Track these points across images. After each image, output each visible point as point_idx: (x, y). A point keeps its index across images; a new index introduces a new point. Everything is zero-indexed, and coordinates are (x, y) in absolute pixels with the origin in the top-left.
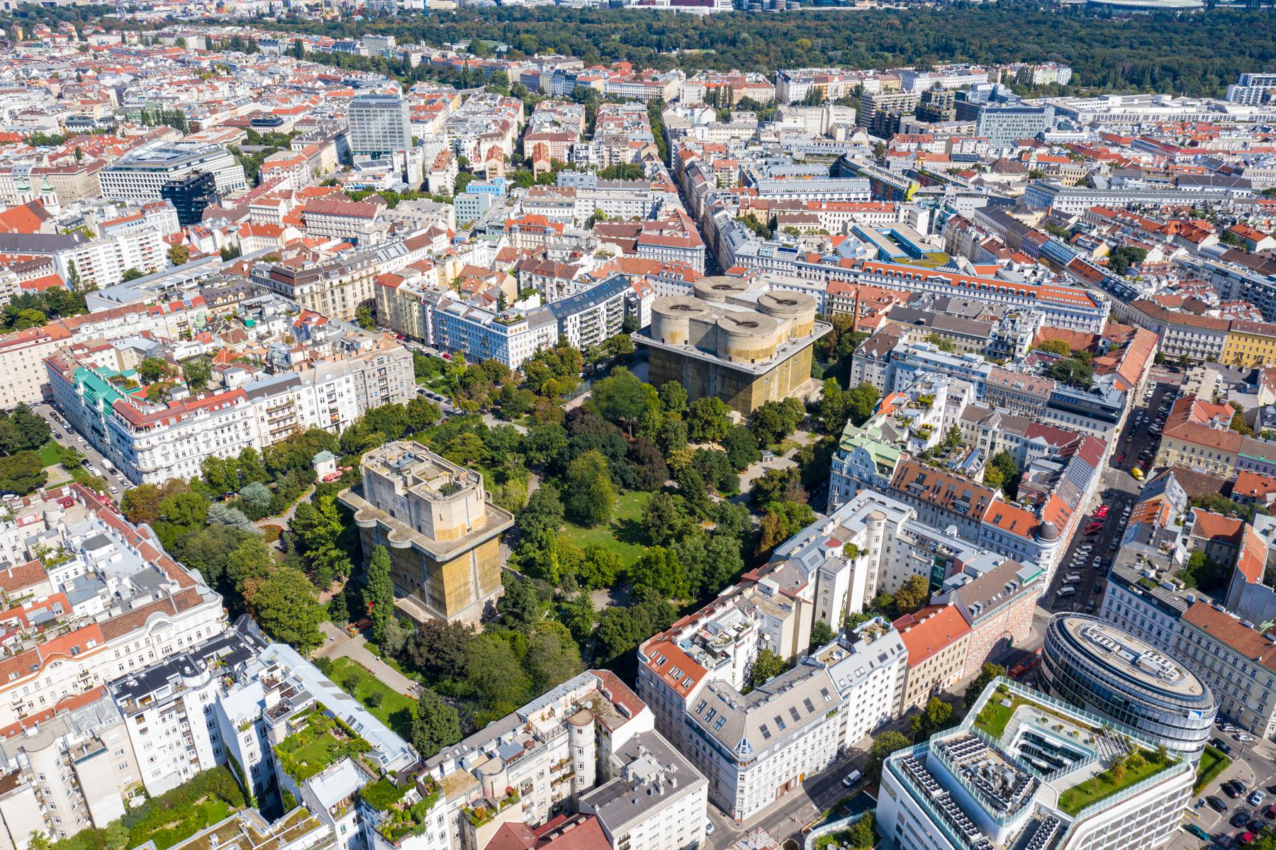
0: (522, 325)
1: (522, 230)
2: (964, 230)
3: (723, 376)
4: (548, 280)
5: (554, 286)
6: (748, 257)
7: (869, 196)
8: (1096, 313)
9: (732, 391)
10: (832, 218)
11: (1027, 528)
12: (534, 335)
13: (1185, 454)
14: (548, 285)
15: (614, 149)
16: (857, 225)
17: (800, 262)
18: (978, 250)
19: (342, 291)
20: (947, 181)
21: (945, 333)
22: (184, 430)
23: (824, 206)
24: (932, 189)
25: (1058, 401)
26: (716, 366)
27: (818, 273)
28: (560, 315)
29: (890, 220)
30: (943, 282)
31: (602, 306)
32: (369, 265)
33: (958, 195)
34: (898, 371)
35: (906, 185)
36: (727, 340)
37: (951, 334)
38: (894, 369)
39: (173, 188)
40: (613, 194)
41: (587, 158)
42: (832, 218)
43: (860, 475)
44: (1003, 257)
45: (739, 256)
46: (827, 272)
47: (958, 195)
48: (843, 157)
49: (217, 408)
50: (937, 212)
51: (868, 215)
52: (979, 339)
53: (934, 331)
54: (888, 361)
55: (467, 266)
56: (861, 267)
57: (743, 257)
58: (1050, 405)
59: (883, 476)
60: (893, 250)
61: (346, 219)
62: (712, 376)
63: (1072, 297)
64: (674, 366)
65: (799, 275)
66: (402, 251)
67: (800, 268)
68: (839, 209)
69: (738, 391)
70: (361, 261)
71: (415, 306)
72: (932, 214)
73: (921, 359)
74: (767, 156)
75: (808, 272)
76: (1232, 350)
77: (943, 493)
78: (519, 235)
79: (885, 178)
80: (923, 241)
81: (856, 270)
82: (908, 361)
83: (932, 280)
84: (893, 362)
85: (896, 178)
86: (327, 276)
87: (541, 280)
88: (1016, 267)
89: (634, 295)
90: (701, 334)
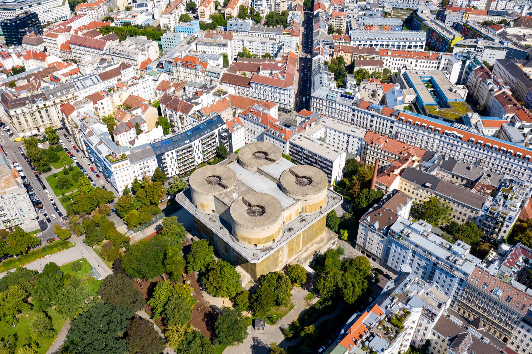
0: (124, 162)
1: (183, 65)
2: (484, 81)
4: (174, 113)
6: (320, 99)
10: (395, 62)
12: (137, 167)
14: (175, 116)
17: (354, 107)
19: (47, 111)
20: (481, 36)
21: (445, 199)
23: (390, 53)
24: (469, 42)
28: (159, 152)
29: (434, 65)
30: (456, 137)
31: (197, 142)
32: (68, 93)
33: (486, 47)
34: (393, 245)
35: (451, 37)
37: (450, 200)
39: (6, 24)
42: (395, 62)
44: (510, 112)
45: (315, 98)
46: (373, 116)
47: (486, 47)
48: (416, 11)
50: (468, 62)
51: (419, 61)
53: (437, 195)
55: (131, 97)
56: (396, 117)
57: (317, 98)
60: (428, 99)
61: (90, 49)
66: (96, 81)
67: (354, 110)
70: (61, 91)
72: (464, 62)
73: (412, 243)
74: (367, 9)
75: (359, 114)
78: (181, 68)
79: (439, 30)
80: (451, 90)
81: (393, 118)
82: (403, 242)
83: (448, 134)
85: (446, 30)
86: (34, 102)
89: (226, 131)
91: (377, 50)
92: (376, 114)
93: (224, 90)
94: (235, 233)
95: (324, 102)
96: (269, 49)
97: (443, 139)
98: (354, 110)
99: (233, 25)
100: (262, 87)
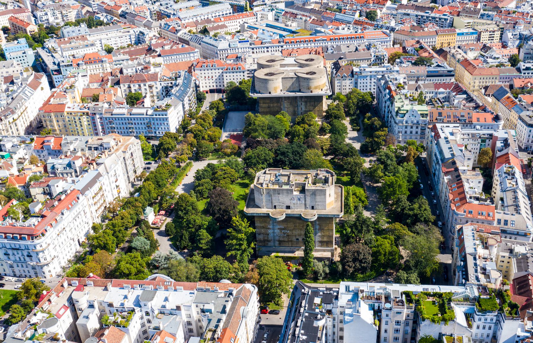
3: (306, 102)
4: (142, 85)
5: (147, 87)
6: (225, 50)
7: (231, 11)
8: (389, 39)
9: (312, 108)
11: (491, 120)
13: (481, 81)
14: (143, 87)
15: (64, 12)
16: (249, 25)
18: (307, 25)
22: (60, 227)
25: (430, 74)
26: (301, 97)
27: (263, 50)
30: (323, 40)
36: (309, 82)
38: (357, 80)
40: (110, 35)
41: (48, 20)
43: (412, 122)
46: (267, 48)
49: (70, 206)
52: (368, 59)
54: (353, 77)
57: (222, 50)
58: (428, 76)
59: (424, 119)
62: (299, 103)
63: (377, 35)
64: (275, 105)
65: (268, 51)
67: (253, 49)
68: (230, 19)
69: (315, 107)
71: (84, 119)
75: (258, 50)
76: (440, 42)
77: (452, 117)
81: (282, 44)
82: (363, 74)
83: (318, 41)
84: (356, 76)
87: (137, 86)
88: (340, 28)
90: (289, 84)
91: (212, 19)
92: (270, 45)
93: (158, 63)
94: (73, 332)
95: (229, 51)
96: (126, 40)
97: (316, 44)
98: (253, 49)
99: (71, 32)
100: (173, 57)
